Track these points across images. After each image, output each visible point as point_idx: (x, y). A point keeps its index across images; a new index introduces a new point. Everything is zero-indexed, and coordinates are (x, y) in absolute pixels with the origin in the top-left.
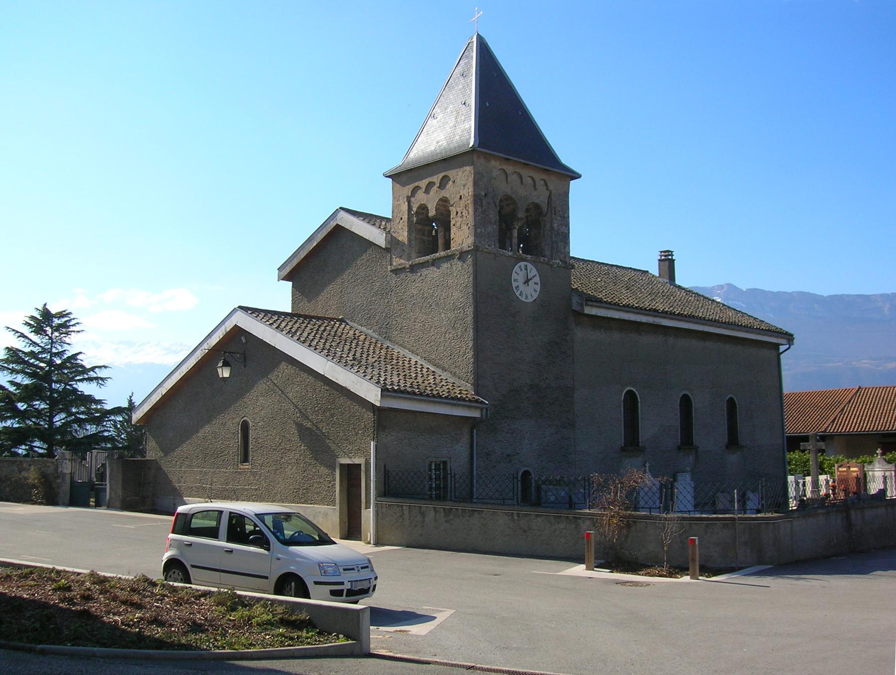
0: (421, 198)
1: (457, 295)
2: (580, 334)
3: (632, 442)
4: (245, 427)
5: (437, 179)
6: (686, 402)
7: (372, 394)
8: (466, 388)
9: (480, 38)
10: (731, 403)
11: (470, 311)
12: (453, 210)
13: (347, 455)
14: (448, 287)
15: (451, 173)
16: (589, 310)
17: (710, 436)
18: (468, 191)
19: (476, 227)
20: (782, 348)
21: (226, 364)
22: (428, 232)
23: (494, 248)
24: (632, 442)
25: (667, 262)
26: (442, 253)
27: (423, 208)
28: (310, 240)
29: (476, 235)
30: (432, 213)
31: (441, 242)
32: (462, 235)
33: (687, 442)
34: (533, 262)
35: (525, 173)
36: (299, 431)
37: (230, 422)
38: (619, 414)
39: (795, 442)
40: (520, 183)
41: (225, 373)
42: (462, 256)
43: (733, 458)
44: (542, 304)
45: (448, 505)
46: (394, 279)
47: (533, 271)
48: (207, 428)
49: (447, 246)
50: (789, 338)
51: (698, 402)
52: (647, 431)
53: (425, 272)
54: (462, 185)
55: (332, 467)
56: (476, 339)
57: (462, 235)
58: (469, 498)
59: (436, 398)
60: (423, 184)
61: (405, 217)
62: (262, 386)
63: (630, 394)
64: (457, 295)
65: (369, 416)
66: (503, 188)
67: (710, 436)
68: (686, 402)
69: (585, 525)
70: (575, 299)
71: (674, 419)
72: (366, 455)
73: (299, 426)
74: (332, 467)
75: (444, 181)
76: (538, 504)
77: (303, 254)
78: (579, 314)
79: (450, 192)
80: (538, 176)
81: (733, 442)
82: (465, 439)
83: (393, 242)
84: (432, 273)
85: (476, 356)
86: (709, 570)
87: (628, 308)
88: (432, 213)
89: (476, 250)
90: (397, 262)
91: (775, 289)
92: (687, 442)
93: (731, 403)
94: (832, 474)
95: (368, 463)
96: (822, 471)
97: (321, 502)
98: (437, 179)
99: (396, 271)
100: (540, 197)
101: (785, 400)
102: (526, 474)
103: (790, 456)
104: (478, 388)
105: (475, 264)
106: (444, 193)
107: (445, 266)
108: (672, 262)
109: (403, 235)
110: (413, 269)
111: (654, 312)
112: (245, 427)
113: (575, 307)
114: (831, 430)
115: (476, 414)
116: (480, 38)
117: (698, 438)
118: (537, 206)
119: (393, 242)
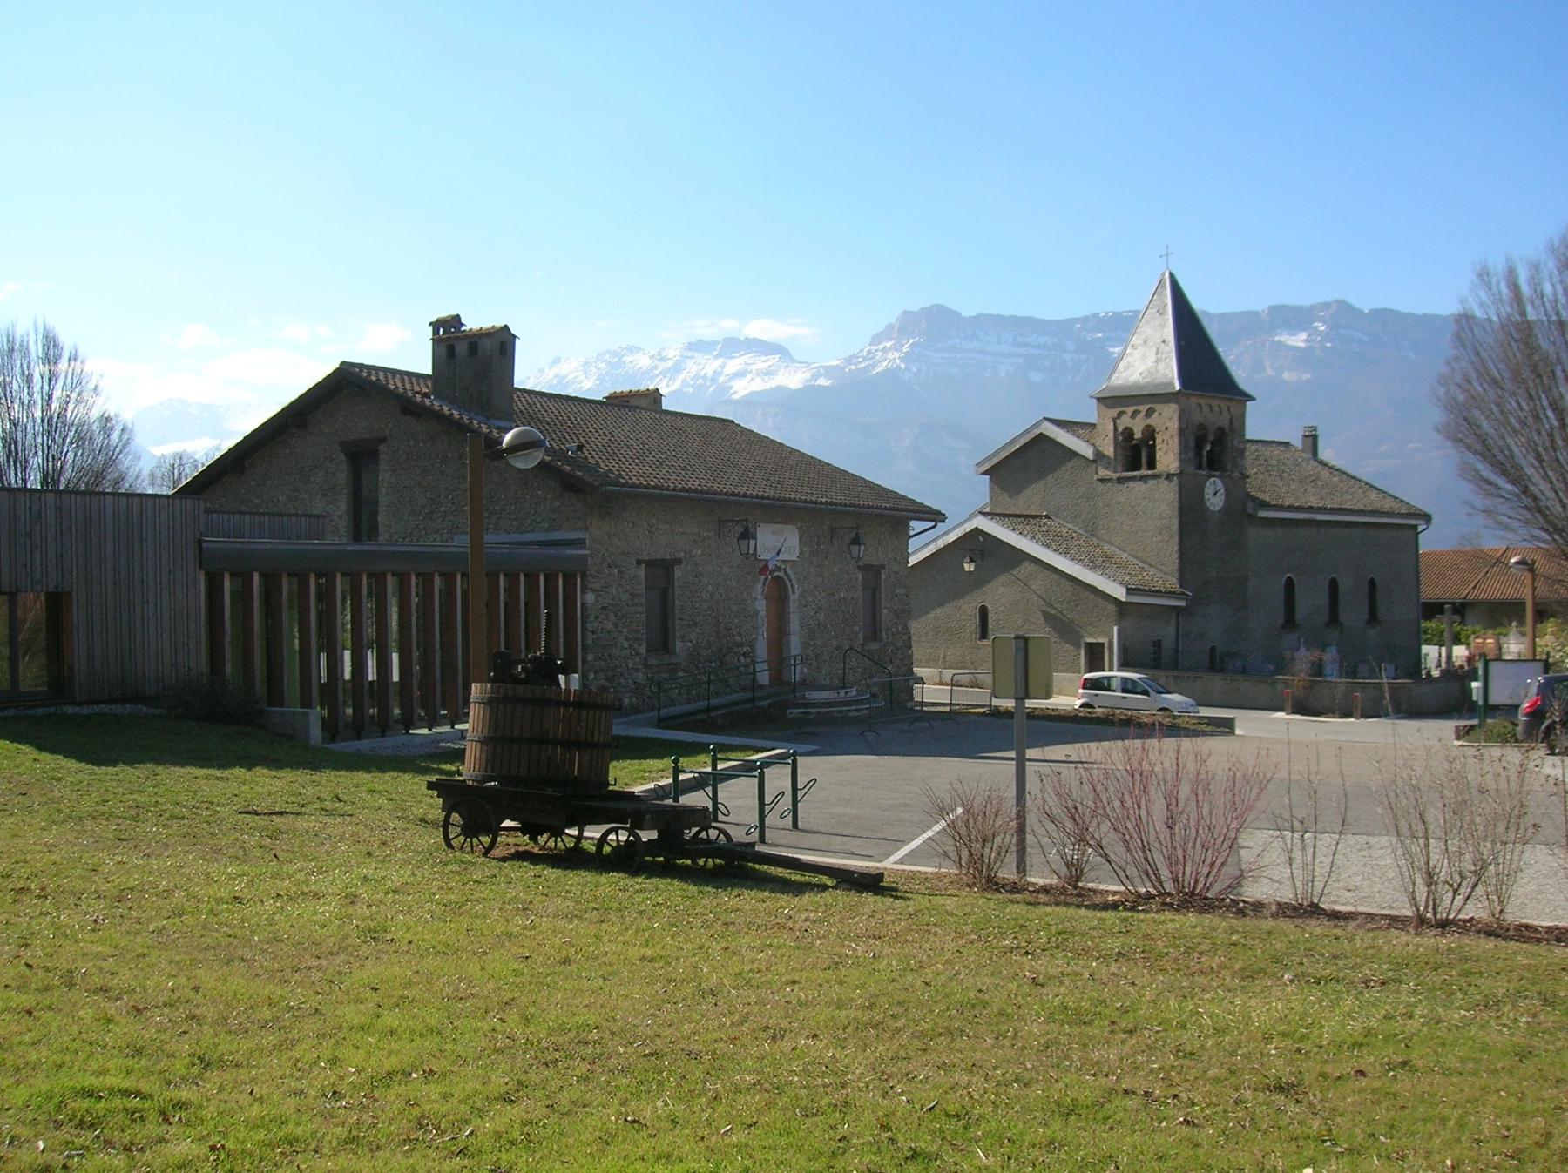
0: (1125, 422)
1: (1163, 507)
2: (1252, 532)
3: (1290, 622)
4: (983, 612)
5: (1143, 408)
6: (1334, 585)
7: (1120, 593)
8: (1172, 583)
9: (1171, 275)
10: (1372, 583)
11: (1176, 522)
12: (1159, 438)
13: (1091, 635)
14: (1152, 505)
15: (1157, 406)
16: (1263, 514)
17: (1353, 612)
18: (1174, 425)
19: (1181, 453)
20: (1420, 528)
21: (972, 560)
22: (1136, 454)
23: (1191, 469)
24: (1290, 622)
25: (1312, 439)
26: (1144, 472)
27: (1129, 433)
28: (1011, 442)
29: (1181, 461)
30: (1138, 435)
31: (1144, 460)
32: (1168, 457)
33: (1334, 619)
34: (1220, 477)
35: (1215, 403)
36: (1046, 619)
37: (967, 608)
38: (1282, 595)
39: (1432, 609)
40: (1211, 411)
41: (969, 567)
42: (1169, 477)
43: (1372, 632)
44: (1225, 510)
45: (1176, 673)
46: (1101, 486)
47: (1220, 485)
48: (939, 611)
49: (1152, 464)
50: (1427, 518)
51: (1345, 583)
52: (1301, 612)
53: (1131, 484)
54: (1167, 421)
55: (1078, 647)
56: (1181, 543)
57: (1168, 457)
58: (1174, 665)
59: (1158, 593)
60: (1130, 410)
61: (1111, 435)
62: (1003, 578)
63: (1290, 580)
64: (1163, 507)
65: (1112, 608)
66: (1198, 418)
67: (1353, 612)
68: (1334, 585)
69: (1280, 686)
70: (1250, 505)
71: (1322, 599)
72: (1111, 636)
73: (1044, 613)
74: (1078, 647)
75: (1149, 413)
76: (1222, 670)
77: (1004, 454)
78: (1252, 517)
79: (1154, 421)
80: (1223, 405)
81: (1373, 618)
82: (1173, 622)
83: (1099, 456)
84: (1139, 487)
85: (1181, 558)
86: (1366, 715)
87: (1291, 508)
88: (1138, 435)
89: (1181, 474)
90: (1103, 473)
91: (1419, 310)
92: (1334, 619)
93: (1372, 583)
94: (1468, 645)
95: (1111, 642)
96: (1457, 641)
97: (1067, 671)
98: (1143, 408)
99: (1102, 480)
100: (1223, 421)
101: (1422, 565)
102: (1213, 649)
103: (1425, 624)
104: (1182, 582)
105: (1181, 485)
106: (1149, 422)
107: (1152, 482)
108: (1315, 437)
109: (1110, 451)
110: (1119, 480)
111: (1311, 509)
112: (983, 612)
113: (1250, 511)
114: (1472, 597)
115: (1182, 604)
116: (1171, 275)
117: (1344, 617)
118: (1221, 429)
119: (1099, 456)
